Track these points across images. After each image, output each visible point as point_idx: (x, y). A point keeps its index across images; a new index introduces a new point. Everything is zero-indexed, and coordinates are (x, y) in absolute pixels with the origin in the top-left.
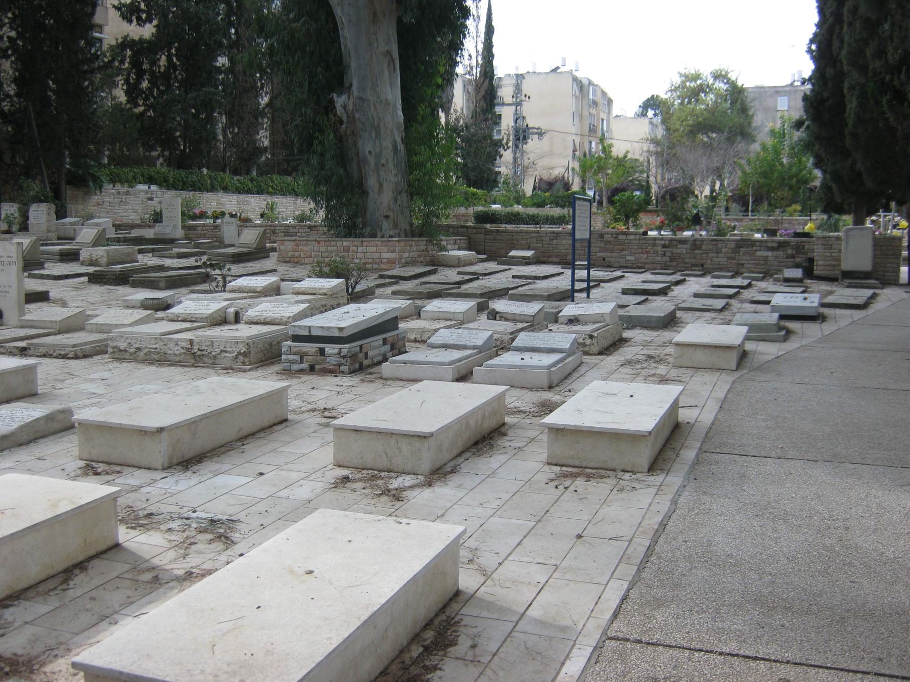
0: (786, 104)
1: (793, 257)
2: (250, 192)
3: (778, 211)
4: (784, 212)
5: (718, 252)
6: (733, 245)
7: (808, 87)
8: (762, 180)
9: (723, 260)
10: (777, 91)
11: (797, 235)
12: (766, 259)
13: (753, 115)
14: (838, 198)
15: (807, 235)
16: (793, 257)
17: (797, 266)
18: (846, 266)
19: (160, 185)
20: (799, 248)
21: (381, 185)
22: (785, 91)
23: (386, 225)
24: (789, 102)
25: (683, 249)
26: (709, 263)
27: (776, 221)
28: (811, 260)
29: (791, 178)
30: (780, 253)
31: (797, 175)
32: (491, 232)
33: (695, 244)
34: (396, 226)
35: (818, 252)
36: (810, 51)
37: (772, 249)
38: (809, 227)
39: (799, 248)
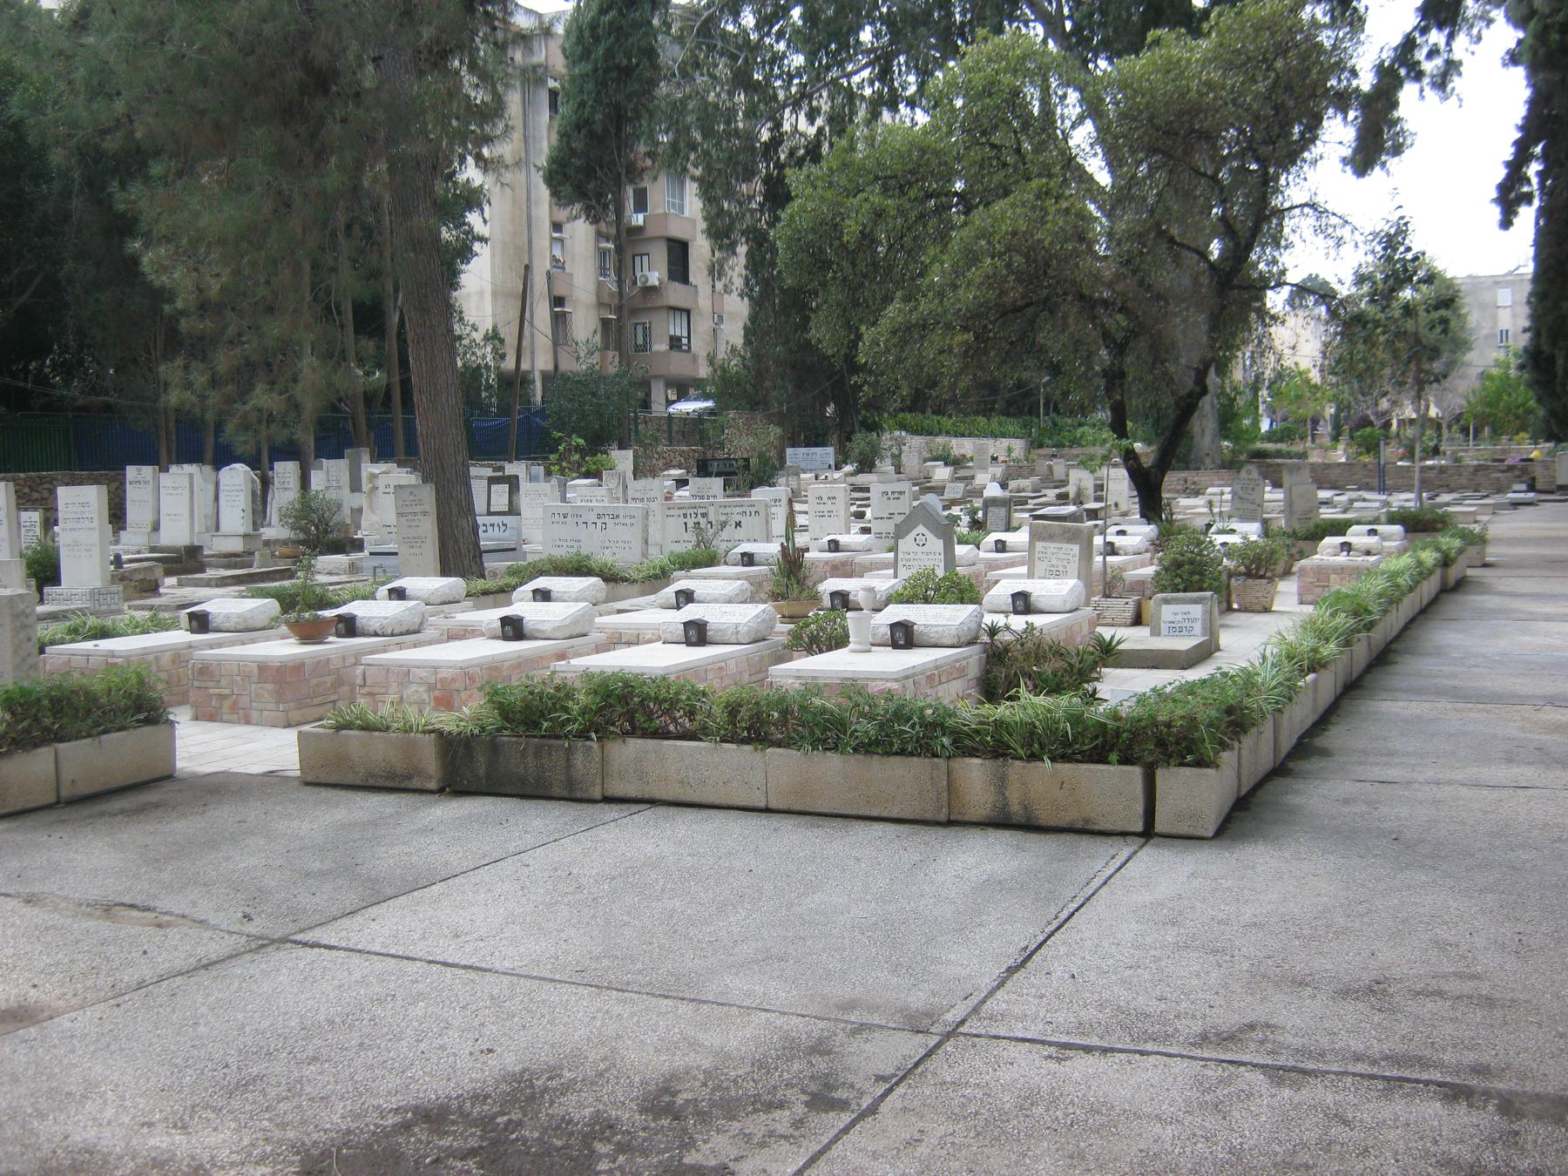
0: (1509, 297)
1: (1519, 477)
2: (963, 435)
3: (1504, 438)
4: (1510, 440)
5: (1460, 475)
6: (1471, 469)
7: (1528, 336)
8: (1488, 410)
9: (1464, 481)
10: (1497, 282)
11: (1522, 460)
12: (1498, 479)
13: (1467, 314)
14: (1555, 429)
15: (1531, 460)
16: (1519, 477)
17: (1522, 482)
18: (1560, 482)
19: (907, 431)
20: (1524, 471)
21: (1203, 431)
22: (1507, 282)
23: (1208, 461)
24: (1513, 295)
25: (1432, 474)
26: (1452, 485)
27: (1504, 451)
28: (1534, 479)
29: (1518, 407)
30: (1509, 474)
31: (1523, 405)
32: (1272, 465)
33: (1442, 470)
34: (1213, 462)
35: (1538, 472)
36: (1529, 302)
37: (1503, 471)
38: (1534, 455)
39: (1524, 471)
